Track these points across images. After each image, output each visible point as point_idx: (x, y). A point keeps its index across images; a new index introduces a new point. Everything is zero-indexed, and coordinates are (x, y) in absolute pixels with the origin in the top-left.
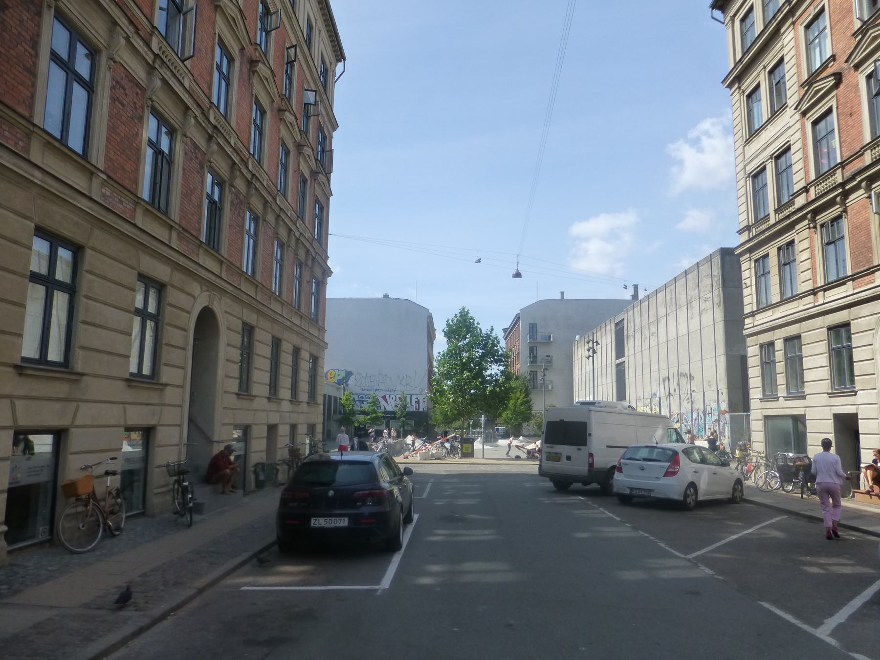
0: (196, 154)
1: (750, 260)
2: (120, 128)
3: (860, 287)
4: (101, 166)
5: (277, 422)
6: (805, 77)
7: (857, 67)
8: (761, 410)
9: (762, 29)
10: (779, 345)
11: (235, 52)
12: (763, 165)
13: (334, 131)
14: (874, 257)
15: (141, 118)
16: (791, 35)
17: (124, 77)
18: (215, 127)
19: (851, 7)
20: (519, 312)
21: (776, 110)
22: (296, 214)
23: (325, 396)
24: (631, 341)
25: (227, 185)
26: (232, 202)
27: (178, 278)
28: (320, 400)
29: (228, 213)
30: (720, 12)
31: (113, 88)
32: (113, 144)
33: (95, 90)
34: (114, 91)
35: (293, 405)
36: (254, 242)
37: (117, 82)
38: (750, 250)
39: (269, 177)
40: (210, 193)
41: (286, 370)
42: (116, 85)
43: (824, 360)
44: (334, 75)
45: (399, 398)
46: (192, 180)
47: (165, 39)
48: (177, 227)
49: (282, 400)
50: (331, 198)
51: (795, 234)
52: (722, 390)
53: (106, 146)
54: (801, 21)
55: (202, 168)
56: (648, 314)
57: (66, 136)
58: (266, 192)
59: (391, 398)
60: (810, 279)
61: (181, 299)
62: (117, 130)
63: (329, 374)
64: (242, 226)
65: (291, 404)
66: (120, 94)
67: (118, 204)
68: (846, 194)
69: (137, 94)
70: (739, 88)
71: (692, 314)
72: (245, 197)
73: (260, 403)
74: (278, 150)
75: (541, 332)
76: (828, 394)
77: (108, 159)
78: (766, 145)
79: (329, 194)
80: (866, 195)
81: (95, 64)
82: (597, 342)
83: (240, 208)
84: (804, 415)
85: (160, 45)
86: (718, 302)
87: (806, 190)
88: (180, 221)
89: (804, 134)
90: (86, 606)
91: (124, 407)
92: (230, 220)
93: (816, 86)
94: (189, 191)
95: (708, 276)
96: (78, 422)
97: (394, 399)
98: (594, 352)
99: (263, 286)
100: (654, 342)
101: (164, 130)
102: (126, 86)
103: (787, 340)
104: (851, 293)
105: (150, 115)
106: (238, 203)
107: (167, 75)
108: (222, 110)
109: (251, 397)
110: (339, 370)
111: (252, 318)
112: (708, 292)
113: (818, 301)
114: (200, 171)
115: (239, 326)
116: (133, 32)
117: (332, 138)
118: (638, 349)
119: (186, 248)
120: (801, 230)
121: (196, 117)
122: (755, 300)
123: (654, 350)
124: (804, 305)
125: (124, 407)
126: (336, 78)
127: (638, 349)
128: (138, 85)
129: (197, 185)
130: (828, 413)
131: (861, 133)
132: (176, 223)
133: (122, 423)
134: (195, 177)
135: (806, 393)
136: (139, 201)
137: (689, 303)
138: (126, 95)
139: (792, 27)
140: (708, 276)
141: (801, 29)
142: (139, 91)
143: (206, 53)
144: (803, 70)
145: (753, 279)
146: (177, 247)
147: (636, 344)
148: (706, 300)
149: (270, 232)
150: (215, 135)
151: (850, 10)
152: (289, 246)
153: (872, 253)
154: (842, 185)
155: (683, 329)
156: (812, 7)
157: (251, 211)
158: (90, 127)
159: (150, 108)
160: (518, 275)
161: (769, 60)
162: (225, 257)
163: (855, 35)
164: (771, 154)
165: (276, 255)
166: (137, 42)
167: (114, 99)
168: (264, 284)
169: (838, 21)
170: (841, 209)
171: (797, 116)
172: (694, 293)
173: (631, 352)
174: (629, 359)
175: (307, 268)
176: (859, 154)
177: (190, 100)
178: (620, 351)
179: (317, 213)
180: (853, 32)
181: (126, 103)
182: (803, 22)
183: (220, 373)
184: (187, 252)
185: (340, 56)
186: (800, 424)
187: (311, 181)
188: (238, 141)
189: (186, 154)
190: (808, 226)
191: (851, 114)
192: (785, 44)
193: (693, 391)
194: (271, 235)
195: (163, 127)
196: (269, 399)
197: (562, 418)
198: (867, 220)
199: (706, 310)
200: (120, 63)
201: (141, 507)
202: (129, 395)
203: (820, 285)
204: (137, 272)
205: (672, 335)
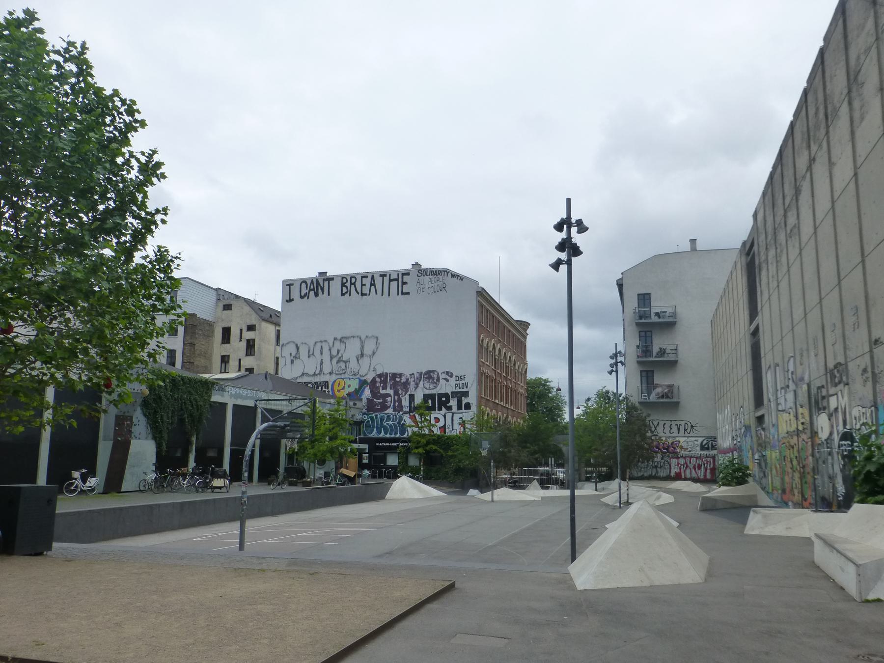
20: (620, 276)
45: (435, 418)
71: (862, 107)
75: (657, 306)
110: (350, 379)
147: (770, 274)
197: (792, 116)
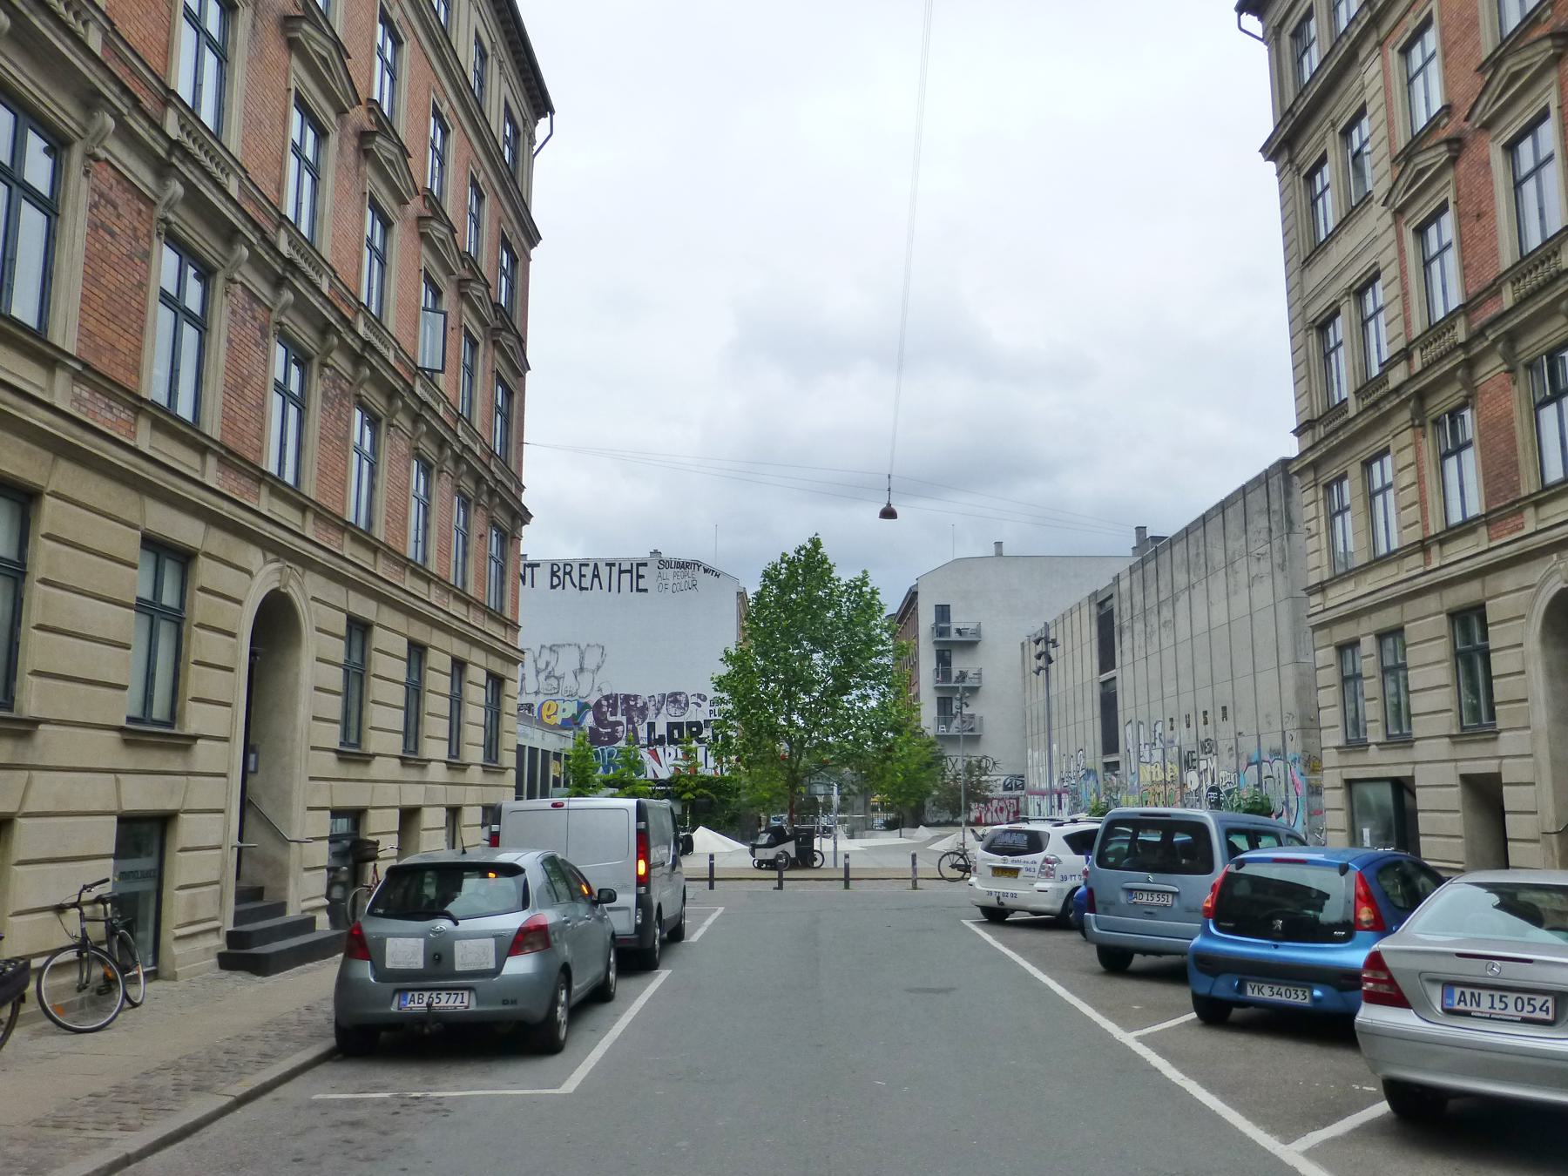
0: (252, 310)
1: (1316, 485)
2: (107, 275)
3: (1499, 537)
4: (71, 348)
5: (421, 803)
6: (1401, 144)
7: (1487, 126)
8: (1339, 770)
9: (1327, 51)
10: (1368, 645)
11: (329, 119)
12: (1334, 307)
13: (532, 248)
14: (1521, 481)
15: (147, 255)
16: (1377, 66)
17: (114, 183)
18: (289, 262)
19: (1476, 17)
21: (1354, 204)
22: (455, 409)
23: (520, 748)
24: (1127, 637)
25: (316, 362)
26: (324, 395)
27: (217, 541)
28: (508, 759)
29: (317, 416)
30: (1256, 18)
31: (94, 206)
32: (95, 306)
33: (60, 212)
34: (95, 211)
35: (452, 772)
36: (371, 465)
37: (101, 195)
38: (1315, 466)
39: (398, 344)
40: (281, 380)
41: (436, 704)
42: (101, 199)
43: (1442, 674)
44: (532, 142)
46: (246, 359)
47: (191, 111)
48: (216, 448)
49: (430, 761)
50: (528, 375)
51: (1390, 437)
52: (1292, 732)
53: (81, 309)
54: (1392, 39)
55: (265, 335)
56: (1155, 586)
57: (7, 301)
58: (391, 373)
59: (667, 754)
60: (1417, 522)
61: (225, 579)
62: (102, 280)
63: (545, 707)
64: (346, 439)
65: (449, 768)
66: (107, 215)
67: (103, 412)
68: (1470, 364)
69: (140, 212)
70: (1291, 161)
71: (1235, 586)
72: (350, 383)
73: (385, 768)
74: (418, 290)
75: (957, 620)
76: (1450, 736)
77: (86, 334)
78: (1338, 270)
79: (523, 367)
80: (1505, 367)
81: (61, 166)
82: (1054, 641)
83: (342, 405)
84: (1412, 778)
85: (182, 122)
86: (1280, 561)
87: (1405, 354)
88: (222, 435)
89: (1401, 251)
90: (39, 1124)
91: (117, 780)
92: (322, 428)
93: (1421, 161)
94: (239, 379)
95: (1260, 512)
96: (30, 807)
97: (673, 755)
98: (1050, 661)
99: (389, 548)
100: (1167, 642)
101: (191, 271)
102: (119, 202)
103: (1381, 636)
104: (1485, 547)
105: (164, 246)
106: (336, 396)
107: (193, 176)
108: (304, 229)
109: (366, 759)
111: (365, 608)
112: (1262, 543)
113: (1430, 563)
114: (261, 341)
115: (340, 624)
116: (130, 106)
117: (529, 259)
118: (1140, 654)
119: (235, 484)
120: (1400, 430)
121: (250, 246)
122: (1325, 561)
123: (1168, 654)
124: (1407, 571)
125: (117, 780)
126: (536, 148)
127: (1140, 654)
128: (141, 196)
129: (256, 368)
130: (1451, 774)
131: (1495, 252)
132: (215, 442)
133: (114, 808)
134: (252, 352)
135: (1415, 736)
136: (143, 405)
137: (1229, 564)
138: (119, 216)
139: (1377, 51)
140: (1260, 512)
141: (1393, 56)
142: (142, 207)
143: (272, 126)
144: (1397, 133)
145: (1322, 519)
146: (218, 484)
148: (1259, 559)
149: (403, 447)
150: (288, 275)
151: (1474, 23)
152: (441, 471)
153: (1518, 475)
154: (1465, 346)
155: (1219, 614)
156: (1411, 16)
157: (363, 407)
158: (51, 278)
159: (163, 237)
160: (888, 514)
161: (1340, 110)
162: (312, 497)
163: (1481, 69)
164: (1346, 286)
165: (414, 487)
166: (136, 121)
167: (95, 227)
168: (392, 544)
169: (1455, 43)
170: (1464, 393)
171: (1388, 218)
172: (1236, 545)
173: (1128, 658)
174: (1126, 676)
175: (480, 510)
176: (1493, 290)
177: (239, 216)
178: (1107, 659)
179: (500, 403)
180: (1479, 63)
181: (116, 230)
182: (1397, 43)
183: (304, 711)
184: (237, 492)
185: (540, 104)
186: (1407, 797)
187: (485, 345)
188: (336, 281)
189: (234, 312)
190: (1410, 423)
191: (1478, 216)
192: (1366, 83)
193: (1240, 734)
194: (406, 451)
195: (189, 267)
196: (404, 761)
198: (1509, 413)
199: (1258, 577)
200: (107, 161)
201: (150, 961)
202: (126, 759)
203: (1433, 533)
204: (139, 533)
205: (1200, 625)
